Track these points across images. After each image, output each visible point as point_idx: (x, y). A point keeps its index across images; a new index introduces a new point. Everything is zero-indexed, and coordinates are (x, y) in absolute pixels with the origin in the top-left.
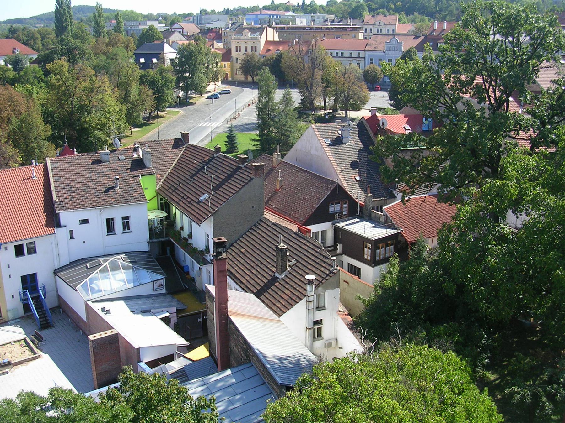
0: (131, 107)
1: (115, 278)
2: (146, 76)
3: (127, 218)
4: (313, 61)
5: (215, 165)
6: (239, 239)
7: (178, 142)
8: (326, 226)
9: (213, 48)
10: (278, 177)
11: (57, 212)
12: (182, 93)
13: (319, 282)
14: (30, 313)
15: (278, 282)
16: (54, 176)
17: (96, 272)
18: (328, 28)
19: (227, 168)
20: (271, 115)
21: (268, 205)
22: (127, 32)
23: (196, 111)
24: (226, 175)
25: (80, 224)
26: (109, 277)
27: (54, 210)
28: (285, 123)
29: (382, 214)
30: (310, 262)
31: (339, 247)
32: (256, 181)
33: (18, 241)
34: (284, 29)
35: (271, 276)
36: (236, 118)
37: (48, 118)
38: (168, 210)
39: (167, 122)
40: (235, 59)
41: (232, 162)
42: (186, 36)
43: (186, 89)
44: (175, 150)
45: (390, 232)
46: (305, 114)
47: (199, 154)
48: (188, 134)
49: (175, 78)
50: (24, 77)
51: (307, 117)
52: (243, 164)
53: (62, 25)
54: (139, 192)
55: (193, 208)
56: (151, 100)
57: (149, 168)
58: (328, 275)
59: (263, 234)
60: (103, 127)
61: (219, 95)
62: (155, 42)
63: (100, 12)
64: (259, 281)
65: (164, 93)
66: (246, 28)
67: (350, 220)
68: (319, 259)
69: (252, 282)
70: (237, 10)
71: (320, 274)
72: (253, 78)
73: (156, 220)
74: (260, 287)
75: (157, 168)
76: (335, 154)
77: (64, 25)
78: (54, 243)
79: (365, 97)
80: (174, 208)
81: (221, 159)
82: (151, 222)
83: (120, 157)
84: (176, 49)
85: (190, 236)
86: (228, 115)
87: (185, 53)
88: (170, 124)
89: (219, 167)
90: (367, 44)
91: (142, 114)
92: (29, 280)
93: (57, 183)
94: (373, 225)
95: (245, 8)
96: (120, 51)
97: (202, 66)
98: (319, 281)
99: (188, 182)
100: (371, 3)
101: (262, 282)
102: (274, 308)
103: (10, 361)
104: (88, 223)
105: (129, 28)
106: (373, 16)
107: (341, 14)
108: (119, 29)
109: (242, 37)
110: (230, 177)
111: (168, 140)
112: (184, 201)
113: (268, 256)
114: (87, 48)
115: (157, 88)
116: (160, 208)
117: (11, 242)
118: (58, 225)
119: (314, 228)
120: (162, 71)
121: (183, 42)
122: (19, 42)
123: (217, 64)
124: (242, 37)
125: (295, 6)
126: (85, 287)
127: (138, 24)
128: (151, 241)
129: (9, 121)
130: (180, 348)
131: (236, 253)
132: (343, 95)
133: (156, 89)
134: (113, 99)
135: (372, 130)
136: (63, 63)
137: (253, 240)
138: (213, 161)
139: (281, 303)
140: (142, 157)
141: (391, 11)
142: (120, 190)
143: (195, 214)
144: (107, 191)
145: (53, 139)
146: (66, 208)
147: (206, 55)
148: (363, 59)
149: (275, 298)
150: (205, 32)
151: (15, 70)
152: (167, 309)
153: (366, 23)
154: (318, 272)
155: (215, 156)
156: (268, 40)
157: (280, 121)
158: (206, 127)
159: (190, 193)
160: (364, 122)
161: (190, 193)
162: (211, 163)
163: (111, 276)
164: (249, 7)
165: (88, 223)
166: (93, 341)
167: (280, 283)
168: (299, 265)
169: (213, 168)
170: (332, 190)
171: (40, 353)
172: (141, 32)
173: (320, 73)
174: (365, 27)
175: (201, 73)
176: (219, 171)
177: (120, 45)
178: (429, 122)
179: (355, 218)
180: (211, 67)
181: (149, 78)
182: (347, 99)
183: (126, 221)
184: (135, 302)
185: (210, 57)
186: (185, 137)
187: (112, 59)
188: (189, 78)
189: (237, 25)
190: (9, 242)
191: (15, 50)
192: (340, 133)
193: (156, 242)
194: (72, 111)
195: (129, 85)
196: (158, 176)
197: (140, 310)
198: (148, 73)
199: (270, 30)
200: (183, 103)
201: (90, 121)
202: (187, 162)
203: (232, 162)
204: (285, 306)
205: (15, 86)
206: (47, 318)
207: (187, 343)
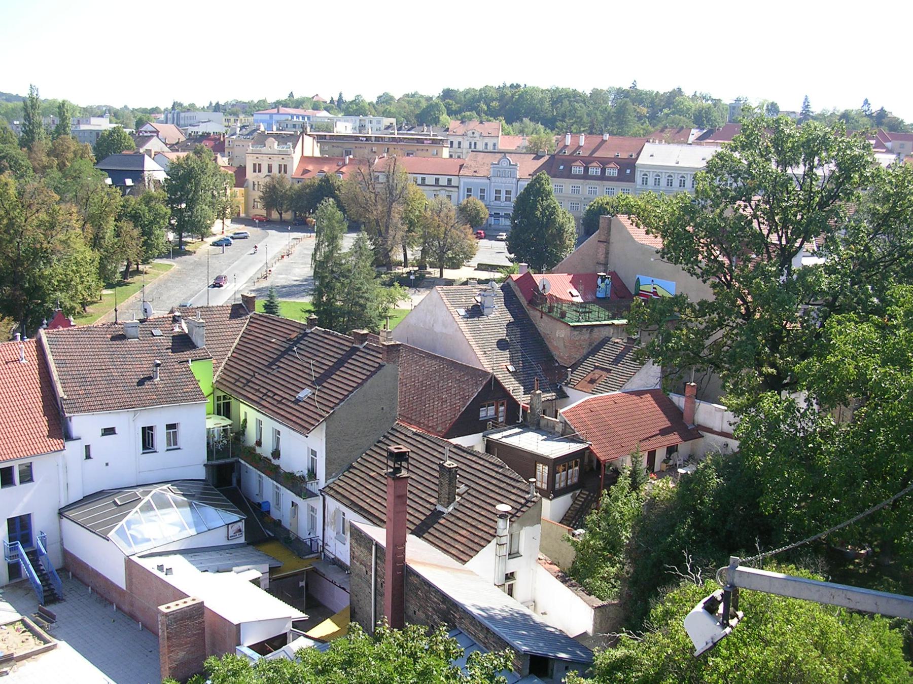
4: (390, 189)
8: (473, 441)
11: (67, 415)
17: (134, 510)
18: (394, 139)
19: (335, 349)
23: (198, 264)
24: (335, 360)
25: (103, 435)
30: (491, 488)
32: (389, 368)
35: (430, 510)
36: (266, 277)
45: (575, 447)
47: (278, 328)
52: (362, 344)
54: (193, 386)
56: (137, 245)
57: (202, 349)
58: (523, 505)
60: (67, 285)
61: (231, 240)
62: (124, 152)
67: (510, 429)
68: (504, 482)
70: (233, 106)
72: (281, 214)
73: (216, 430)
76: (475, 331)
79: (471, 246)
81: (319, 336)
83: (155, 332)
85: (276, 454)
86: (252, 272)
88: (160, 285)
89: (318, 348)
90: (461, 166)
92: (18, 525)
93: (62, 369)
94: (545, 437)
100: (451, 102)
103: (12, 654)
104: (115, 433)
110: (340, 363)
118: (68, 437)
124: (264, 150)
126: (122, 533)
128: (210, 462)
130: (296, 624)
132: (436, 243)
135: (525, 296)
139: (457, 548)
140: (187, 332)
142: (162, 382)
143: (294, 419)
144: (141, 383)
146: (81, 410)
148: (456, 189)
149: (445, 542)
153: (451, 133)
155: (308, 331)
156: (305, 155)
160: (512, 284)
165: (115, 433)
166: (166, 615)
171: (55, 641)
174: (451, 139)
178: (607, 285)
179: (515, 427)
181: (129, 210)
182: (442, 250)
183: (171, 431)
189: (249, 130)
192: (479, 301)
199: (308, 140)
200: (178, 251)
202: (259, 340)
204: (464, 553)
206: (52, 587)
207: (304, 615)
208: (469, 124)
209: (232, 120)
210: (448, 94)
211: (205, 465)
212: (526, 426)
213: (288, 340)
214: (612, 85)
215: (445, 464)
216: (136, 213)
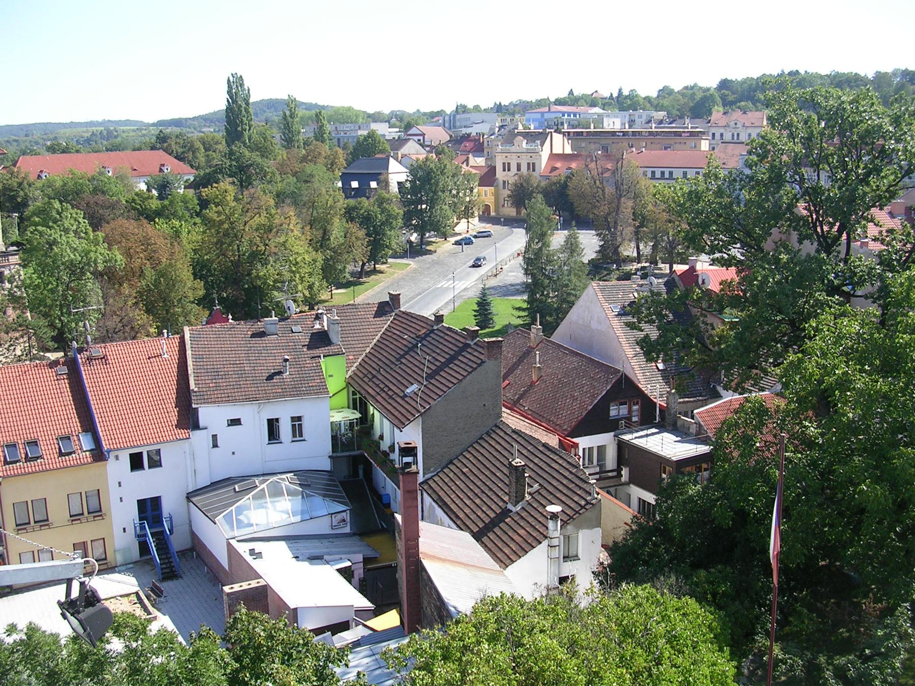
0: (331, 256)
1: (275, 507)
2: (357, 208)
3: (299, 418)
5: (433, 342)
6: (462, 454)
7: (383, 307)
8: (605, 439)
9: (467, 165)
10: (535, 363)
11: (194, 406)
12: (415, 235)
13: (568, 518)
14: (149, 557)
15: (510, 517)
16: (194, 353)
17: (247, 497)
20: (546, 270)
21: (518, 405)
22: (339, 140)
24: (447, 356)
25: (229, 425)
26: (265, 505)
27: (191, 405)
28: (567, 282)
29: (693, 421)
31: (625, 472)
33: (135, 447)
34: (582, 135)
36: (496, 276)
37: (200, 270)
38: (363, 409)
39: (389, 280)
40: (502, 183)
41: (458, 338)
42: (428, 146)
43: (421, 229)
44: (378, 319)
45: (703, 449)
46: (605, 269)
47: (414, 325)
48: (399, 294)
49: (401, 212)
50: (169, 208)
51: (608, 274)
53: (236, 129)
54: (319, 381)
55: (395, 405)
56: (362, 245)
58: (582, 507)
59: (498, 447)
61: (473, 239)
62: (377, 156)
63: (293, 110)
64: (482, 516)
65: (384, 235)
66: (520, 134)
67: (642, 430)
68: (573, 483)
69: (473, 517)
70: (515, 105)
71: (573, 505)
74: (483, 525)
75: (349, 346)
77: (239, 129)
78: (188, 452)
80: (371, 408)
82: (335, 427)
84: (407, 168)
87: (420, 173)
91: (350, 268)
93: (198, 364)
94: (679, 439)
95: (528, 102)
96: (318, 170)
97: (447, 193)
98: (568, 515)
99: (393, 366)
100: (726, 92)
101: (487, 518)
102: (500, 555)
104: (240, 424)
105: (342, 134)
106: (725, 113)
107: (678, 110)
108: (322, 136)
109: (513, 149)
111: (369, 304)
112: (384, 395)
113: (500, 479)
114: (270, 165)
115: (374, 227)
116: (351, 406)
117: (125, 448)
118: (196, 426)
119: (584, 442)
120: (381, 202)
121: (417, 156)
122: (170, 155)
123: (472, 191)
124: (513, 149)
125: (606, 98)
126: (229, 519)
127: (357, 127)
128: (335, 455)
129: (142, 274)
130: (360, 612)
131: (455, 474)
132: (665, 238)
133: (372, 229)
134: (302, 243)
136: (227, 186)
137: (482, 455)
138: (432, 335)
141: (758, 104)
143: (396, 413)
144: (270, 378)
145: (205, 302)
146: (207, 402)
147: (453, 176)
150: (459, 141)
151: (161, 197)
152: (349, 556)
153: (714, 125)
154: (569, 502)
155: (435, 327)
156: (554, 152)
157: (559, 278)
158: (447, 289)
159: (393, 384)
160: (677, 278)
161: (393, 384)
162: (428, 339)
163: (269, 505)
164: (534, 101)
165: (240, 424)
166: (228, 594)
167: (513, 519)
168: (544, 492)
169: (430, 346)
170: (615, 383)
172: (355, 140)
173: (630, 203)
174: (713, 130)
175: (445, 204)
176: (438, 351)
177: (321, 160)
179: (652, 428)
180: (461, 195)
181: (362, 212)
183: (297, 423)
184: (302, 544)
185: (461, 179)
186: (395, 299)
187: (306, 182)
188: (426, 212)
190: (121, 449)
191: (163, 168)
193: (344, 456)
194: (239, 260)
195: (329, 222)
196: (351, 357)
197: (308, 556)
198: (360, 203)
199: (557, 138)
200: (415, 251)
201: (265, 275)
202: (394, 336)
203: (458, 338)
204: (515, 553)
205: (155, 222)
206: (172, 564)
207: (371, 605)
208: (731, 114)
209: (509, 119)
210: (725, 84)
211: (329, 457)
212: (663, 427)
213: (417, 337)
214: (897, 67)
215: (513, 463)
216: (368, 214)
